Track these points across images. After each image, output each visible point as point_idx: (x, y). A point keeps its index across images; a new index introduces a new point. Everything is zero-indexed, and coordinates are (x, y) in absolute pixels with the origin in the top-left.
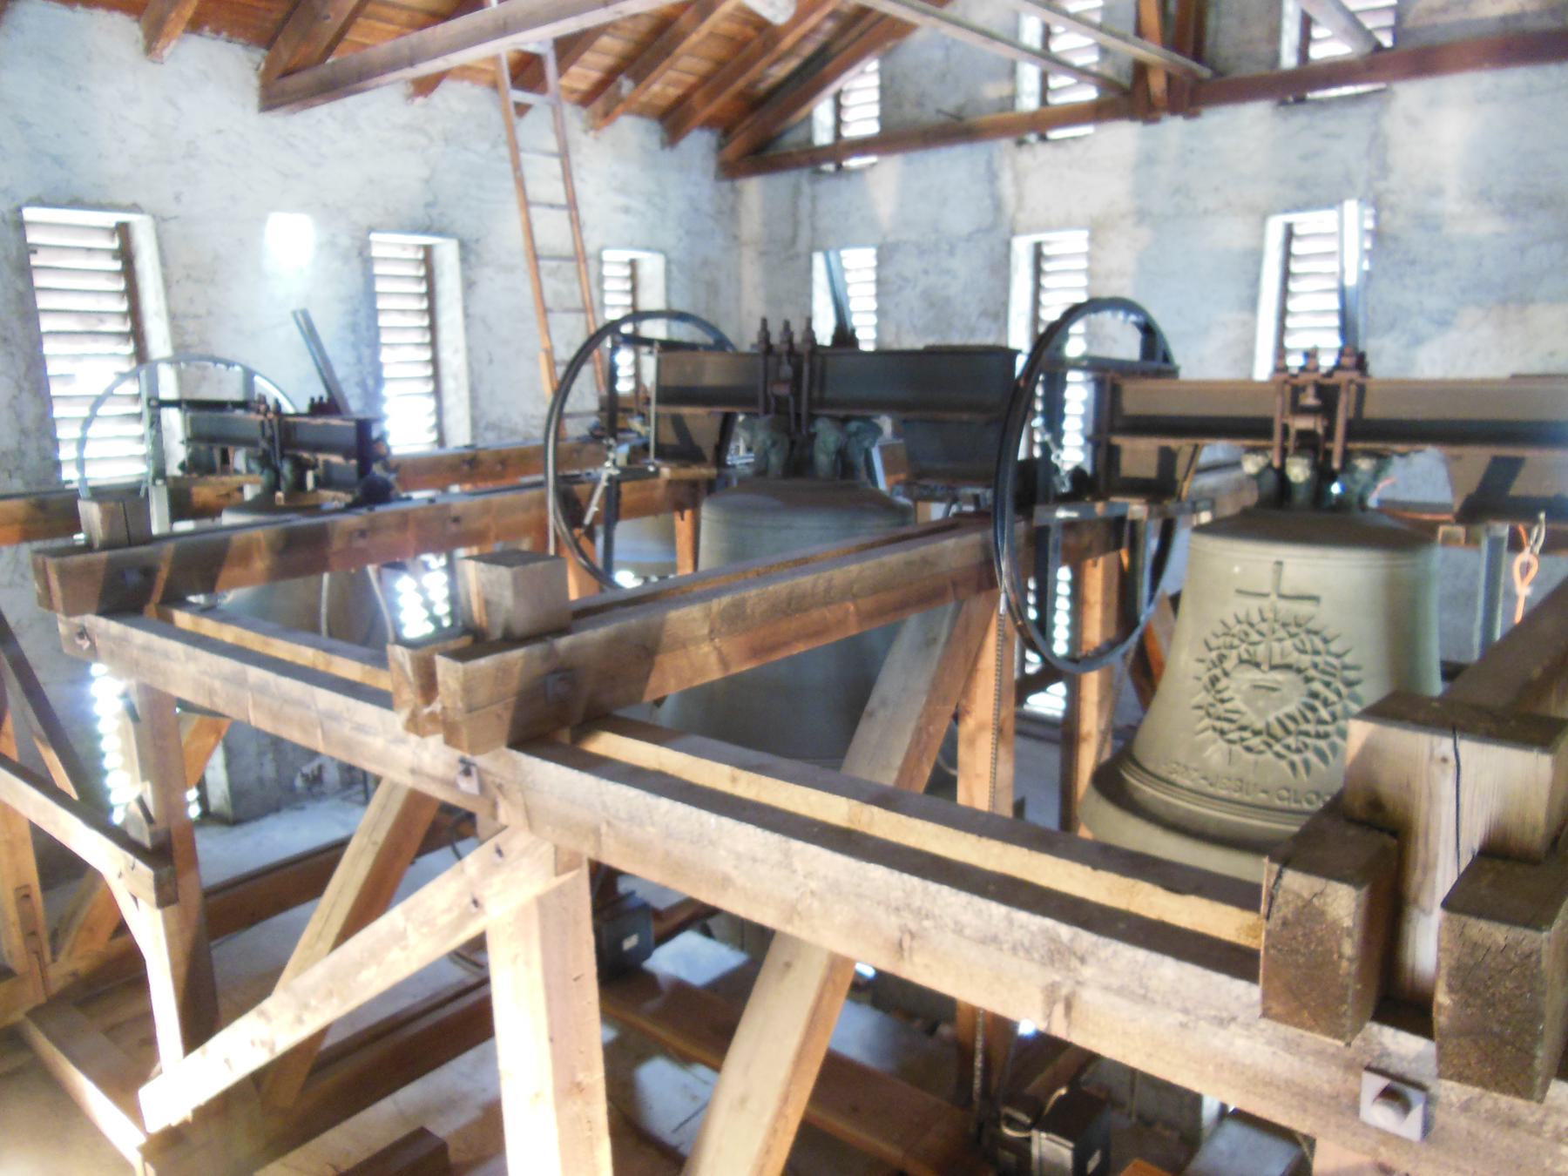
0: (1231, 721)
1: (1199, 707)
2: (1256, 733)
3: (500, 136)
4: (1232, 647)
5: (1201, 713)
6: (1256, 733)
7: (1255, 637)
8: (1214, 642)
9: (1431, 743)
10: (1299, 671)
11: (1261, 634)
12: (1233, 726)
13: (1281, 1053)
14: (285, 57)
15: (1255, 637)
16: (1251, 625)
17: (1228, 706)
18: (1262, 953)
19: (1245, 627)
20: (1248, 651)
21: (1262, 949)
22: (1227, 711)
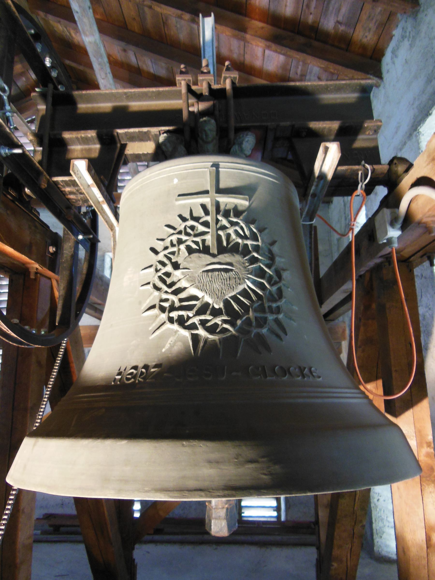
0: (189, 308)
1: (153, 307)
2: (216, 313)
3: (378, 500)
4: (180, 242)
5: (156, 311)
6: (216, 313)
7: (201, 228)
8: (159, 246)
9: (344, 201)
10: (245, 251)
11: (206, 224)
12: (190, 314)
13: (422, 9)
14: (240, 525)
15: (201, 228)
16: (196, 219)
17: (183, 295)
18: (210, 191)
19: (191, 223)
20: (196, 243)
21: (223, 308)
22: (181, 300)
